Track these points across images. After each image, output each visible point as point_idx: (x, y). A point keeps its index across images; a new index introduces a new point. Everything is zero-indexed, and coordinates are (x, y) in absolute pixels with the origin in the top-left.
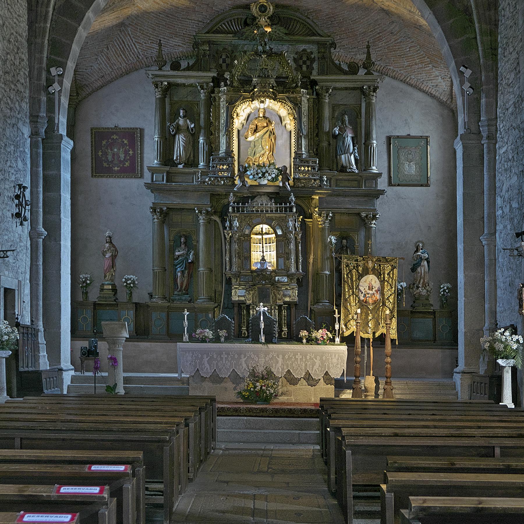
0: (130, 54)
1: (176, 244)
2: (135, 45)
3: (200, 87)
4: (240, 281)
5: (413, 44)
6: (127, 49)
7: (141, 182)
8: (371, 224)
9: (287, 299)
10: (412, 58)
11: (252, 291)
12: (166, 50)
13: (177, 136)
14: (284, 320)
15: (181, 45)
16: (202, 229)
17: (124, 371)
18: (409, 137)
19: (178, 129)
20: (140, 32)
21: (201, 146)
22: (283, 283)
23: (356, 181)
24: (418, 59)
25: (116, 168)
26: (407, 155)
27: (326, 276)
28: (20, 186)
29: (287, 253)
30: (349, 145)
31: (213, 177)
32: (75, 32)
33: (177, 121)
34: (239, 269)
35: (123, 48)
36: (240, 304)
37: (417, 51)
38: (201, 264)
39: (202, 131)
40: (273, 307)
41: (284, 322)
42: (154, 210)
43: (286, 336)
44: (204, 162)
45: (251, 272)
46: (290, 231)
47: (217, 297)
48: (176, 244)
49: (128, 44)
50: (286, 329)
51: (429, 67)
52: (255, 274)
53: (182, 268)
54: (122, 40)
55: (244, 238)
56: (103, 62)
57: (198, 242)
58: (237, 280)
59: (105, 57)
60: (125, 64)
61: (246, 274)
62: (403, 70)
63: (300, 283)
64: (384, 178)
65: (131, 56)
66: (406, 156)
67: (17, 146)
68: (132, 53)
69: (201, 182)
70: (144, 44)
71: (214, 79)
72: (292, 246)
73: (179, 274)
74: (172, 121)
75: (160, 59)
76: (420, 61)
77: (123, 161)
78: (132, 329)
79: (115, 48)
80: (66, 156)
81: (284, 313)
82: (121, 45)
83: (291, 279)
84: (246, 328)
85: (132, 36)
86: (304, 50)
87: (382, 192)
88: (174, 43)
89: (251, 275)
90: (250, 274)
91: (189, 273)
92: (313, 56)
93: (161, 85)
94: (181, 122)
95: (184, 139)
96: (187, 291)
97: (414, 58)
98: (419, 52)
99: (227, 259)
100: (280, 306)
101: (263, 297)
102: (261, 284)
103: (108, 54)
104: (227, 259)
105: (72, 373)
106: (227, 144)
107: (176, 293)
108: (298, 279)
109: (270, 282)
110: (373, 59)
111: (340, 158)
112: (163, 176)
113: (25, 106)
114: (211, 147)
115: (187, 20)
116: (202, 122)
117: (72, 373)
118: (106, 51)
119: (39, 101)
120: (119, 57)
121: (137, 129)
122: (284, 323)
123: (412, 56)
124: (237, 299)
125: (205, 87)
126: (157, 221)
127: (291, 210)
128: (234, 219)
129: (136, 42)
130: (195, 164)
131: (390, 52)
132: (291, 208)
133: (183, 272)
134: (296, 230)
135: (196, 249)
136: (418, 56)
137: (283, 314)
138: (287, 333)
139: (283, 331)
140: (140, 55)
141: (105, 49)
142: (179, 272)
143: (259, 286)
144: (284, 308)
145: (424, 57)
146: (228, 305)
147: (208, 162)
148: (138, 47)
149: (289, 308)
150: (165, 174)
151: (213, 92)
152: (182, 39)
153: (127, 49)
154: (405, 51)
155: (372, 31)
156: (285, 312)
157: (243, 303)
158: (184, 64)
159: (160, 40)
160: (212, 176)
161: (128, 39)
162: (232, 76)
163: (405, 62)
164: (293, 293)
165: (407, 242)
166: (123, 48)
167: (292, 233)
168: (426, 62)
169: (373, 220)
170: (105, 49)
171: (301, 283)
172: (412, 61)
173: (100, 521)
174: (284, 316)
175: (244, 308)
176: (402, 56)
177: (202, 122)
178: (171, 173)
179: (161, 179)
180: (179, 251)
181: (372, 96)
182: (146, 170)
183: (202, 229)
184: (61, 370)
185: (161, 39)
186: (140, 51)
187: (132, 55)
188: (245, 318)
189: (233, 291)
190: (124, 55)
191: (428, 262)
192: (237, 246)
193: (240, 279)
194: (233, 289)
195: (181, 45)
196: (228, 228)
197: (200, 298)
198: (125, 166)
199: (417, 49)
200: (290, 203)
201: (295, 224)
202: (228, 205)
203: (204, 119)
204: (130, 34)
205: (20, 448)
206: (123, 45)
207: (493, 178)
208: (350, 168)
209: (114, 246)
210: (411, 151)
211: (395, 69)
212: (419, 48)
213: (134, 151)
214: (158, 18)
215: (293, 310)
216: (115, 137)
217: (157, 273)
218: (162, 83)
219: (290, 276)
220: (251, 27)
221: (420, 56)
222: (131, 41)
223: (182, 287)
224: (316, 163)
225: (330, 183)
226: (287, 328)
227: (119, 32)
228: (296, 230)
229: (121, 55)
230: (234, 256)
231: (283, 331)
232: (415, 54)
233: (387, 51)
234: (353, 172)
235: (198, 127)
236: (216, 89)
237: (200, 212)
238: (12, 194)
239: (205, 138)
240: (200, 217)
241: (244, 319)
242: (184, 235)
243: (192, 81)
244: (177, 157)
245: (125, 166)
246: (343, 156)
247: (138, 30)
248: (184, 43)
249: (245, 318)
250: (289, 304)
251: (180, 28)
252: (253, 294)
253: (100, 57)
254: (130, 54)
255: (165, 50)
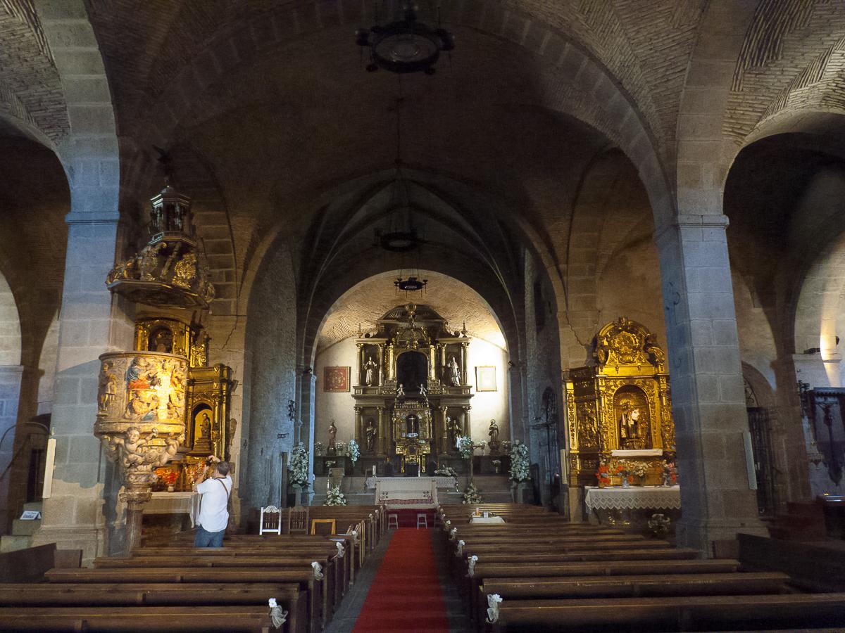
1: (367, 426)
7: (350, 394)
9: (425, 452)
17: (316, 523)
21: (380, 375)
28: (291, 401)
32: (314, 340)
36: (400, 456)
42: (356, 408)
48: (367, 426)
63: (431, 444)
64: (474, 388)
67: (290, 382)
72: (427, 425)
74: (365, 363)
80: (313, 384)
81: (423, 459)
87: (473, 395)
101: (412, 451)
105: (314, 494)
110: (467, 329)
113: (294, 361)
116: (381, 363)
117: (314, 494)
119: (301, 358)
130: (378, 384)
132: (426, 405)
147: (383, 383)
151: (386, 348)
157: (402, 454)
158: (371, 335)
162: (396, 340)
173: (844, 392)
177: (381, 363)
179: (360, 392)
182: (352, 387)
184: (308, 493)
191: (498, 431)
202: (394, 404)
207: (526, 389)
219: (426, 440)
238: (287, 405)
243: (376, 343)
255: (362, 328)
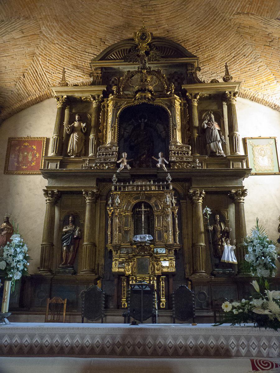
0: (42, 82)
2: (45, 74)
3: (93, 98)
4: (120, 254)
5: (261, 64)
6: (39, 78)
8: (240, 199)
10: (260, 77)
11: (131, 262)
12: (70, 81)
13: (72, 135)
14: (163, 291)
15: (81, 76)
16: (88, 208)
18: (260, 138)
19: (73, 130)
20: (49, 63)
22: (162, 255)
23: (224, 164)
24: (264, 77)
25: (24, 167)
26: (260, 151)
27: (202, 248)
29: (164, 226)
30: (216, 136)
31: (99, 163)
33: (73, 124)
34: (120, 242)
35: (36, 76)
36: (120, 275)
37: (265, 70)
38: (85, 239)
39: (92, 130)
40: (151, 278)
41: (163, 293)
42: (46, 193)
43: (164, 307)
44: (92, 153)
45: (130, 245)
46: (168, 205)
47: (99, 270)
49: (40, 74)
50: (165, 300)
51: (274, 83)
52: (135, 246)
53: (68, 243)
54: (35, 70)
55: (125, 213)
56: (21, 88)
57: (84, 221)
58: (117, 252)
59: (22, 84)
60: (39, 92)
61: (126, 246)
62: (252, 88)
65: (43, 85)
66: (260, 152)
68: (44, 82)
69: (88, 167)
70: (53, 74)
71: (104, 92)
72: (170, 219)
73: (65, 248)
75: (63, 82)
76: (266, 79)
77: (30, 162)
78: (16, 301)
79: (30, 77)
82: (35, 73)
83: (169, 250)
84: (125, 300)
85: (42, 66)
86: (175, 72)
88: (76, 74)
89: (131, 248)
90: (130, 246)
91: (74, 248)
92: (182, 76)
93: (62, 98)
94: (76, 124)
95: (77, 136)
96: (72, 264)
97: (262, 76)
98: (266, 70)
99: (109, 233)
100: (158, 277)
102: (140, 256)
103: (24, 81)
104: (109, 233)
106: (112, 137)
107: (61, 266)
108: (175, 251)
109: (149, 253)
111: (210, 146)
112: (57, 165)
114: (99, 141)
115: (85, 53)
118: (23, 78)
120: (33, 84)
121: (44, 138)
122: (163, 294)
123: (260, 74)
124: (117, 270)
125: (96, 98)
126: (49, 202)
127: (168, 188)
128: (116, 197)
129: (46, 71)
130: (86, 154)
131: (243, 73)
133: (68, 247)
134: (172, 205)
135: (82, 226)
136: (265, 75)
137: (161, 285)
138: (165, 303)
139: (161, 301)
140: (50, 84)
141: (21, 76)
142: (64, 246)
143: (138, 257)
144: (162, 280)
145: (270, 75)
146: (110, 278)
147: (95, 151)
148: (48, 76)
149: (167, 281)
150: (59, 163)
152: (82, 70)
153: (39, 78)
154: (255, 71)
155: (229, 55)
156: (163, 283)
157: (123, 274)
159: (64, 69)
160: (98, 162)
161: (40, 68)
163: (254, 81)
164: (171, 263)
165: (267, 220)
166: (36, 76)
167: (169, 207)
168: (271, 79)
169: (242, 196)
170: (21, 76)
171: (179, 255)
172: (259, 79)
174: (163, 287)
175: (124, 280)
176: (252, 76)
178: (63, 162)
180: (66, 228)
181: (233, 99)
183: (88, 208)
185: (65, 67)
186: (49, 81)
187: (44, 84)
188: (125, 289)
189: (114, 263)
190: (38, 83)
192: (117, 220)
193: (120, 251)
194: (113, 261)
195: (81, 76)
196: (110, 205)
197: (83, 270)
198: (32, 165)
199: (265, 68)
200: (167, 182)
201: (172, 201)
203: (95, 120)
204: (41, 64)
205: (81, 322)
206: (36, 74)
208: (219, 153)
209: (10, 225)
210: (263, 148)
211: (245, 89)
212: (266, 67)
213: (40, 154)
214: (62, 50)
215: (171, 280)
216: (26, 144)
217: (45, 248)
218: (62, 97)
219: (168, 247)
220: (134, 53)
221: (267, 74)
222: (42, 71)
223: (66, 260)
224: (189, 149)
225: (202, 165)
226: (165, 298)
227: (32, 62)
228: (172, 205)
229: (35, 84)
230: (115, 230)
231: (161, 301)
232: (262, 72)
233: (240, 73)
234: (222, 156)
235: (88, 126)
236: (105, 99)
237: (87, 193)
239: (94, 134)
240: (87, 198)
241: (124, 290)
242: (72, 215)
244: (70, 151)
245: (32, 165)
246: (212, 144)
247: (47, 60)
248: (84, 74)
249: (125, 289)
250: (167, 274)
251: (80, 60)
252: (133, 266)
253: (18, 83)
254: (42, 82)
